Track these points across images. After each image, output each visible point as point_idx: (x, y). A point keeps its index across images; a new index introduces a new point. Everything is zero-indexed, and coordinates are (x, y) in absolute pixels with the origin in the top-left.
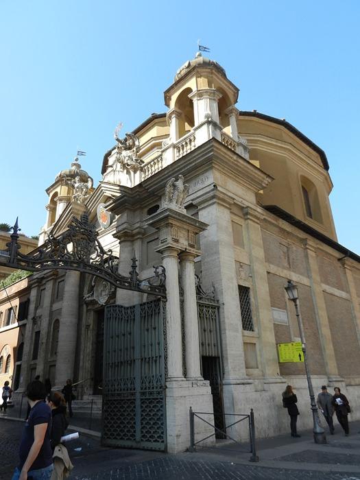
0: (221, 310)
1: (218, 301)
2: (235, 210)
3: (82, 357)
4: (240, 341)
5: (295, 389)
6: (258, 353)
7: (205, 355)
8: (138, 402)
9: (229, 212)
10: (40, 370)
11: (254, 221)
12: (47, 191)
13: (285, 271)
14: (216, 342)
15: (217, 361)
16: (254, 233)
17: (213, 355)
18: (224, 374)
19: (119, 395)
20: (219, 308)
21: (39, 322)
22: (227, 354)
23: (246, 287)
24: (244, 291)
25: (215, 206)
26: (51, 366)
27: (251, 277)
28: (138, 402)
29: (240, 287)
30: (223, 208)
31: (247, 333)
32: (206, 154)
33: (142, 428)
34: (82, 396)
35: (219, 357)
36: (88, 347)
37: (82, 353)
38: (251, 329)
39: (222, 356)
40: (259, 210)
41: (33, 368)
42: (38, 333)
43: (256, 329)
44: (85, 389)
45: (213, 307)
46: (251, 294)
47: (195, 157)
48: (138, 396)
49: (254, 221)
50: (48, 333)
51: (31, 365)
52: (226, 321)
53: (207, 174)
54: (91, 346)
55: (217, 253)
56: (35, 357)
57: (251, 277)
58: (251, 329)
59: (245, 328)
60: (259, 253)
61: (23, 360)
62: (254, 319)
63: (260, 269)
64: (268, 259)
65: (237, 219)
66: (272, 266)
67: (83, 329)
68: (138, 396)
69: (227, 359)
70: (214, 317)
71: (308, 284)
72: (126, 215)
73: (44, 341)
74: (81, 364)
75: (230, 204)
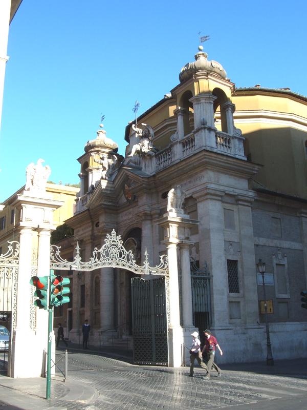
0: (211, 280)
1: (209, 274)
2: (227, 199)
3: (119, 307)
4: (225, 300)
5: (272, 332)
6: (241, 307)
7: (197, 311)
8: (154, 340)
9: (220, 202)
10: (87, 315)
11: (244, 205)
12: (78, 160)
13: (275, 241)
14: (206, 303)
15: (207, 315)
16: (244, 215)
17: (204, 311)
18: (211, 323)
19: (143, 335)
20: (209, 279)
21: (83, 278)
22: (214, 310)
23: (234, 261)
24: (232, 265)
25: (209, 201)
26: (96, 313)
27: (239, 252)
28: (154, 340)
29: (228, 261)
30: (214, 201)
31: (232, 294)
32: (201, 160)
33: (157, 354)
34: (121, 336)
35: (208, 313)
36: (123, 300)
37: (119, 304)
38: (237, 291)
39: (211, 312)
40: (251, 194)
41: (82, 314)
42: (83, 287)
43: (241, 291)
44: (123, 331)
45: (204, 279)
46: (239, 265)
47: (192, 161)
48: (153, 337)
49: (244, 205)
50: (92, 286)
51: (80, 311)
52: (214, 288)
53: (203, 173)
54: (125, 299)
55: (209, 238)
56: (83, 305)
57: (239, 252)
58: (237, 291)
59: (231, 291)
60: (249, 231)
61: (73, 307)
62: (240, 283)
63: (248, 244)
64: (257, 233)
65: (228, 206)
66: (261, 239)
67: (118, 285)
68: (153, 337)
69: (214, 314)
70: (205, 285)
71: (300, 248)
72: (145, 198)
73: (89, 293)
74: (119, 313)
75: (221, 196)
